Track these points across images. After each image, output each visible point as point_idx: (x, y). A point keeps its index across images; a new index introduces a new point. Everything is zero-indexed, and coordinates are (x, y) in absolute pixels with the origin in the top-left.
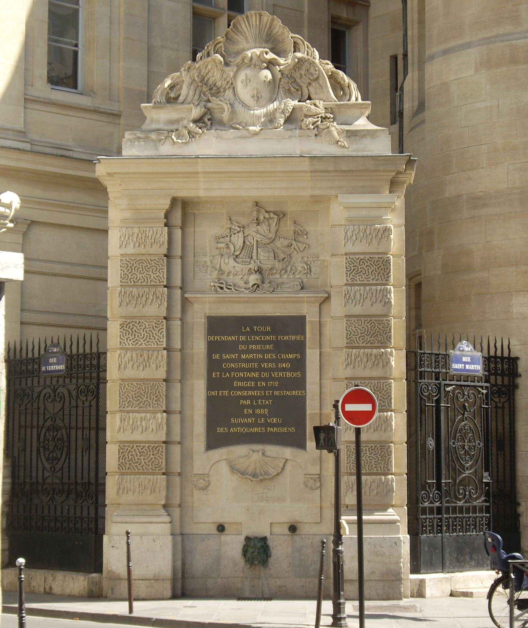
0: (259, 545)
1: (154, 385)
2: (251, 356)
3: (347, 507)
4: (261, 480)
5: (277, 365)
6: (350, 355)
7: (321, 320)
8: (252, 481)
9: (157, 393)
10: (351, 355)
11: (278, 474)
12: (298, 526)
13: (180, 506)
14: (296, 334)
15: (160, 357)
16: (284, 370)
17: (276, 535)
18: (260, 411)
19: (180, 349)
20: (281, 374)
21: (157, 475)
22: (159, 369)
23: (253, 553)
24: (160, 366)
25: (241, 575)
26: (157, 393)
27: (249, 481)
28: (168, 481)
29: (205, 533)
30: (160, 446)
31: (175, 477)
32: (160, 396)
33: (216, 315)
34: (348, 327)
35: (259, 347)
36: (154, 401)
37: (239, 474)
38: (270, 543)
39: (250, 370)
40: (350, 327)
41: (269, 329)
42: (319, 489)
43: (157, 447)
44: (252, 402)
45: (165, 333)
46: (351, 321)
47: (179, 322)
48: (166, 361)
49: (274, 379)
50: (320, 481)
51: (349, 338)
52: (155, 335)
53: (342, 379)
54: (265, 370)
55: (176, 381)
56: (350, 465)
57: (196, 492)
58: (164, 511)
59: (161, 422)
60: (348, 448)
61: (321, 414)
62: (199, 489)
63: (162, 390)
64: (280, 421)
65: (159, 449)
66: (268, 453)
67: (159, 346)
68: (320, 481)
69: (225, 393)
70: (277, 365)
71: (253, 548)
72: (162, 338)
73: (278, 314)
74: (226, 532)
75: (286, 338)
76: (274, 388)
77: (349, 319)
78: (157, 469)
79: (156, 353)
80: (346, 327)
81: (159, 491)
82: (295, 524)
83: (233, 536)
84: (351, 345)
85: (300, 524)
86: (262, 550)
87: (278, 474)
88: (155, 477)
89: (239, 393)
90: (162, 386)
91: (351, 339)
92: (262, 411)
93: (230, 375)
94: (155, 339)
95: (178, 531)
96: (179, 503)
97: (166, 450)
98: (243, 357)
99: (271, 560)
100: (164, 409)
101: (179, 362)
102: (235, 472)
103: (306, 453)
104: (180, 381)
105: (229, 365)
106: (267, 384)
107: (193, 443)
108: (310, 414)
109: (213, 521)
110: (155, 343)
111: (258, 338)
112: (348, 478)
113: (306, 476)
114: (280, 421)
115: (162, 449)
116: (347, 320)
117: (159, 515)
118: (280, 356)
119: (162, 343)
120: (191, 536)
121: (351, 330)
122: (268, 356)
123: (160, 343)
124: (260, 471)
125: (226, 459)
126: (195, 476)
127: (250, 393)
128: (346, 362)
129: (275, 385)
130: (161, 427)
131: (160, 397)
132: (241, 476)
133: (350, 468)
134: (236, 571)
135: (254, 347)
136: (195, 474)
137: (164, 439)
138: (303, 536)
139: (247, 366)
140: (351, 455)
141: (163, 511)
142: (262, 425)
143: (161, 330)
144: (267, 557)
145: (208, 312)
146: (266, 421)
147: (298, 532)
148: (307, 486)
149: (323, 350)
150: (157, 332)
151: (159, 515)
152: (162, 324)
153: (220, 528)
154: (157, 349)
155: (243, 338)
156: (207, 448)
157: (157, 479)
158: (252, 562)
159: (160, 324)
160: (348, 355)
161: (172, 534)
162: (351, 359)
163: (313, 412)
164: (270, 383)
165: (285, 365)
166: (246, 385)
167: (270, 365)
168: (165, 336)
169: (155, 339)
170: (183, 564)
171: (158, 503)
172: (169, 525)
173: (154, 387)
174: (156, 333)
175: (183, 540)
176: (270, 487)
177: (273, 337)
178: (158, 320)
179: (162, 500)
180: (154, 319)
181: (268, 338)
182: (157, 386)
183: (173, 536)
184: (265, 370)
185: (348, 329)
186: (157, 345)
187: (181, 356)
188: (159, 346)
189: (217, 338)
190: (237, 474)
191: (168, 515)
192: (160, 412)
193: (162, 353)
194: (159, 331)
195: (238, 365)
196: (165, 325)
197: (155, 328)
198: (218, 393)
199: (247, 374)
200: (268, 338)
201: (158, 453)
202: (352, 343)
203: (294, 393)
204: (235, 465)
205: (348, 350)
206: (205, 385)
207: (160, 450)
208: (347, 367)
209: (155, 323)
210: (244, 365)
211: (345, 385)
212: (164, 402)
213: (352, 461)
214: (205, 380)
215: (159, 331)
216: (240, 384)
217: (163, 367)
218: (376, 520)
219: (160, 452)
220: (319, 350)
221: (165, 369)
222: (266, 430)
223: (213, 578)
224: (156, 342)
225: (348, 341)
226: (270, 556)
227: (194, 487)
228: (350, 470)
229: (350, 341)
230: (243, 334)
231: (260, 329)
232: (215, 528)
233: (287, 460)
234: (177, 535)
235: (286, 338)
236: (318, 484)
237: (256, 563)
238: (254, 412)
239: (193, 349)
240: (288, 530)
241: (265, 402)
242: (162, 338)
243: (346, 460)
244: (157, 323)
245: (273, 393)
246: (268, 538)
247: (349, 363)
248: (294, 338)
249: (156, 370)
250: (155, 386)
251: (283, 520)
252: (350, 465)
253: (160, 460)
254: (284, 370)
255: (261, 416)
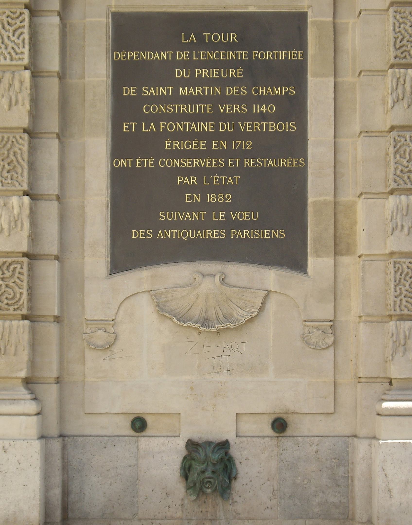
0: (215, 457)
1: (6, 139)
2: (198, 90)
3: (391, 383)
4: (219, 332)
5: (250, 108)
6: (402, 80)
7: (338, 21)
8: (199, 333)
9: (12, 156)
10: (405, 81)
11: (251, 320)
12: (290, 419)
13: (58, 381)
14: (288, 48)
15: (17, 84)
16: (263, 117)
17: (246, 437)
18: (217, 198)
19: (58, 73)
20: (257, 126)
21: (11, 320)
22: (14, 108)
23: (203, 472)
24: (17, 102)
25: (179, 514)
26: (12, 156)
27: (195, 333)
28: (33, 332)
29: (108, 434)
30: (18, 262)
31: (48, 324)
32: (18, 161)
33: (110, 104)
34: (397, 25)
35: (214, 73)
36: (5, 171)
37: (174, 320)
38: (235, 452)
39: (192, 136)
40: (402, 26)
41: (233, 37)
42: (332, 349)
43: (10, 264)
44: (200, 181)
45: (26, 36)
46: (404, 12)
47: (56, 20)
48: (29, 91)
49: (245, 136)
50: (334, 333)
51: (400, 47)
52: (6, 40)
53: (381, 132)
54: (226, 118)
55: (51, 136)
56: (401, 300)
57: (89, 355)
58: (26, 392)
59: (19, 214)
60: (397, 266)
61: (335, 203)
62: (95, 349)
63: (20, 149)
64: (255, 217)
65: (15, 268)
66: (232, 279)
67: (14, 63)
68: (334, 333)
69: (148, 162)
70: (250, 108)
71: (203, 463)
72: (21, 46)
73: (251, 9)
74: (148, 432)
75: (268, 55)
76: (245, 154)
77: (399, 9)
78: (12, 308)
79: (8, 75)
80: (394, 24)
81: (16, 350)
82: (284, 416)
83: (161, 440)
84: (404, 61)
85: (295, 415)
86: (220, 467)
87: (251, 320)
88: (7, 323)
89: (175, 162)
90: (21, 141)
91: (404, 48)
92: (221, 197)
93: (157, 127)
94: (6, 48)
95: (54, 431)
96: (55, 375)
97: (29, 270)
98: (183, 92)
99: (237, 485)
100: (25, 187)
101: (57, 97)
102: (167, 315)
103: (305, 278)
104: (58, 136)
105: (154, 109)
106: (229, 145)
107: (84, 259)
108: (314, 203)
109: (124, 411)
110: (8, 56)
111: (212, 56)
112: (396, 327)
113: (307, 323)
114: (254, 216)
115: (22, 268)
116: (395, 12)
117: (14, 400)
118: (257, 91)
119: (21, 56)
120: (80, 439)
121: (403, 32)
122: (234, 91)
123: (17, 57)
124: (217, 314)
125: (149, 291)
126: (89, 322)
127: (196, 162)
128: (394, 95)
129: (246, 146)
130: (19, 225)
131: (16, 164)
132: (180, 323)
133: (399, 306)
134: (169, 507)
135: (204, 73)
136: (87, 320)
137: (24, 248)
138: (300, 439)
139: (192, 110)
140: (402, 280)
141: (23, 392)
142: (219, 225)
143: (20, 31)
144: (230, 479)
145: (113, 4)
146: (227, 216)
147: (289, 432)
148: (307, 343)
149: (340, 80)
150: (11, 34)
151: (14, 400)
152: (21, 18)
153: (138, 425)
154: (13, 69)
155: (184, 56)
156: (111, 270)
157: (11, 327)
158: (201, 489)
159: (18, 18)
160: (398, 79)
161: (42, 437)
162: (404, 89)
163: (322, 199)
164: (236, 143)
165: (266, 107)
166: (188, 146)
167: (236, 108)
168: (27, 41)
169: (6, 48)
170: (66, 493)
171: (14, 375)
172: (35, 418)
173: (5, 145)
174: (9, 37)
175: (64, 448)
176: (235, 346)
177: (241, 55)
178: (13, 10)
179: (21, 370)
180: (5, 8)
181: (232, 55)
182: (10, 142)
183: (43, 441)
184: (226, 118)
185: (397, 30)
186: (11, 59)
187: (60, 88)
188: (14, 63)
189: (132, 55)
190: (171, 319)
191: (35, 399)
192: (17, 195)
193: (20, 75)
194: (14, 31)
195: (174, 108)
196: (27, 20)
197: (7, 27)
198: (134, 163)
199: (190, 126)
200: (232, 55)
201: (12, 276)
202: (405, 57)
203: (282, 162)
204: (167, 301)
205: (397, 70)
206: (107, 146)
207: (18, 270)
208: (396, 105)
209: (8, 17)
210: (184, 108)
211: (392, 140)
212: (26, 173)
213: (404, 292)
214: (107, 136)
215: (14, 31)
216: (176, 144)
217: (23, 104)
218: (392, 409)
219: (17, 275)
220: (332, 79)
221: (28, 107)
222: (228, 233)
223: (125, 519)
224: (9, 53)
225: (398, 53)
226: (235, 478)
227: (86, 344)
228: (401, 310)
229: (402, 53)
230: (183, 48)
231: (216, 38)
232: (129, 424)
233: (269, 292)
234: (53, 438)
235: (268, 55)
236: (330, 340)
237: (209, 491)
238: (204, 199)
239: (84, 78)
240: (270, 427)
241: (226, 180)
242: (21, 46)
243: (393, 290)
244: (12, 15)
245: (242, 163)
246: (231, 443)
247: (401, 97)
248: (283, 55)
249: (9, 109)
250: (7, 142)
251: (261, 407)
252: (401, 300)
253: (17, 290)
254: (263, 117)
255: (217, 207)
